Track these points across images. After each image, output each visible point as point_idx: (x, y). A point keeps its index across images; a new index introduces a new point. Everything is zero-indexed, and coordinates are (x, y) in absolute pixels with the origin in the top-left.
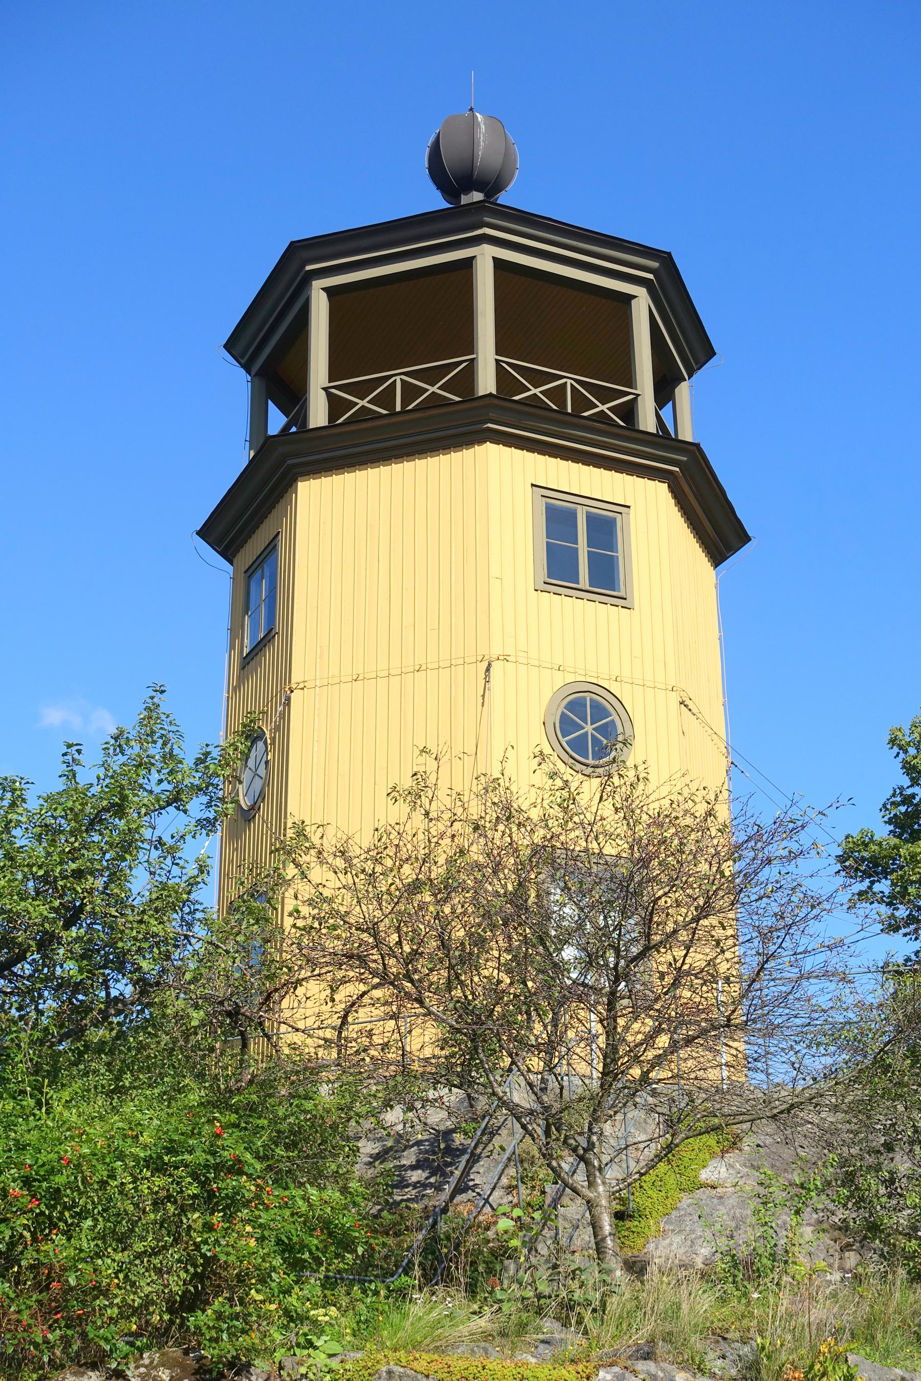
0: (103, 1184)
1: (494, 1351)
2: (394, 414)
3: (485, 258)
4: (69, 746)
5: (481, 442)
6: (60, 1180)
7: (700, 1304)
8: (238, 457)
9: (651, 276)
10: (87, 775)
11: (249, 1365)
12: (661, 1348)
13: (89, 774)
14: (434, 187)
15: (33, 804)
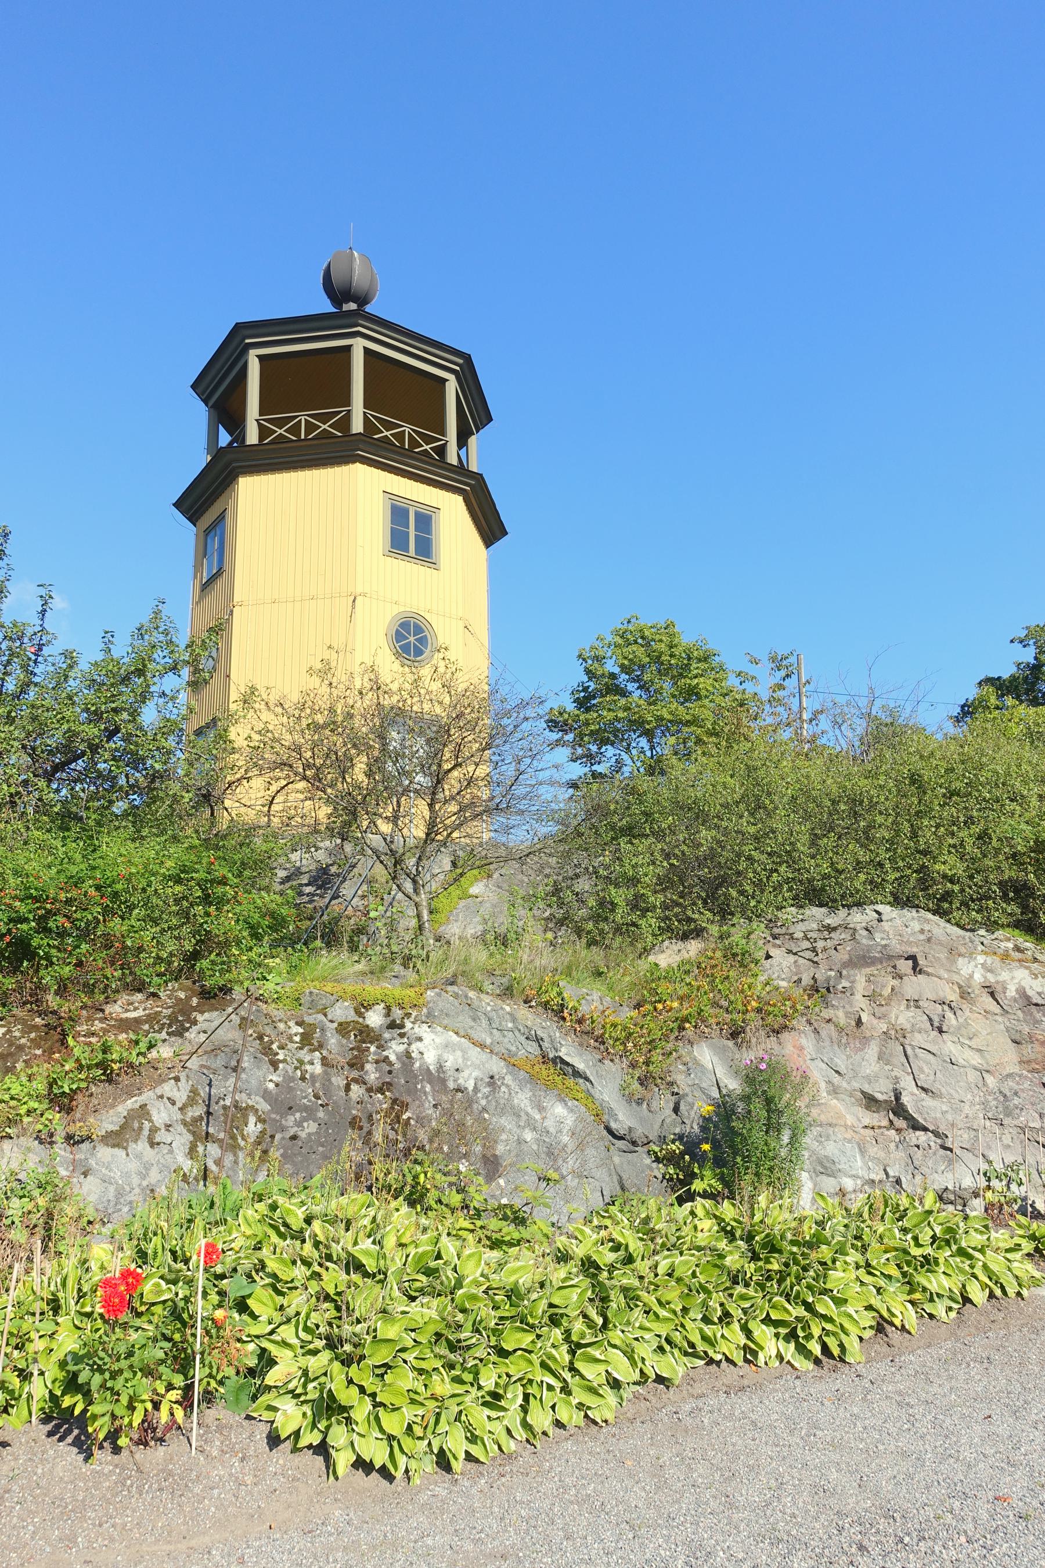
0: (144, 890)
1: (368, 982)
2: (300, 440)
4: (106, 632)
5: (354, 462)
6: (119, 887)
7: (480, 956)
8: (203, 459)
9: (458, 368)
10: (117, 652)
11: (231, 989)
12: (460, 979)
13: (121, 650)
14: (326, 297)
15: (83, 665)
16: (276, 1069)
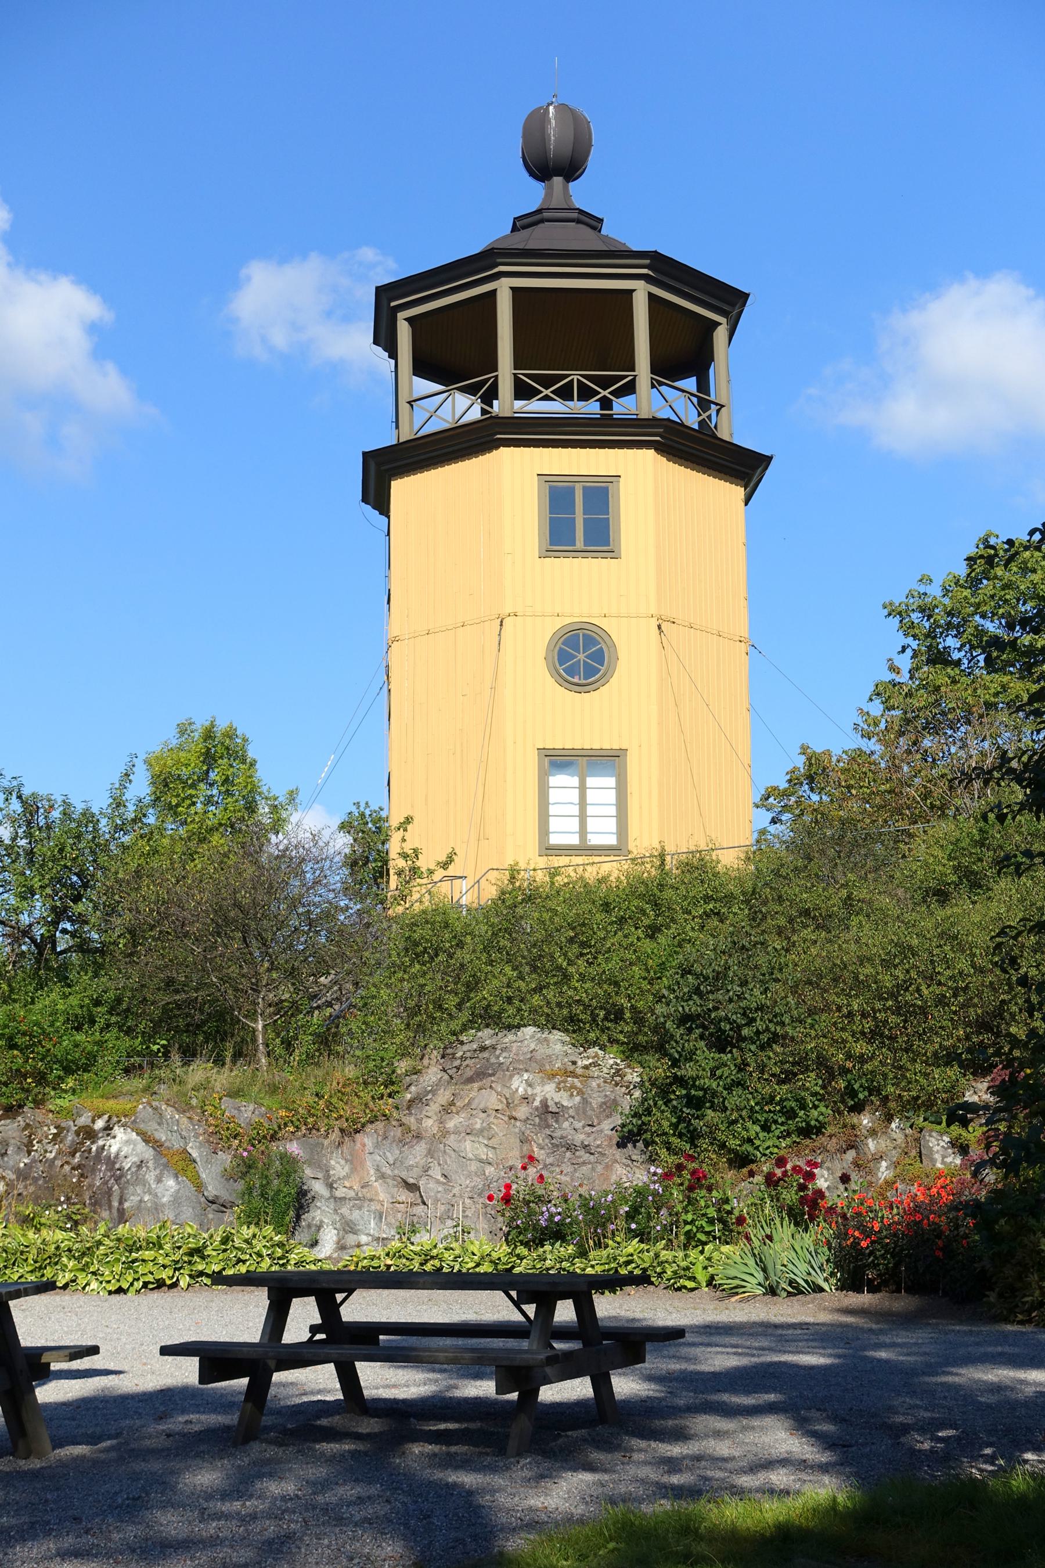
3: (504, 289)
5: (497, 447)
16: (29, 1154)
